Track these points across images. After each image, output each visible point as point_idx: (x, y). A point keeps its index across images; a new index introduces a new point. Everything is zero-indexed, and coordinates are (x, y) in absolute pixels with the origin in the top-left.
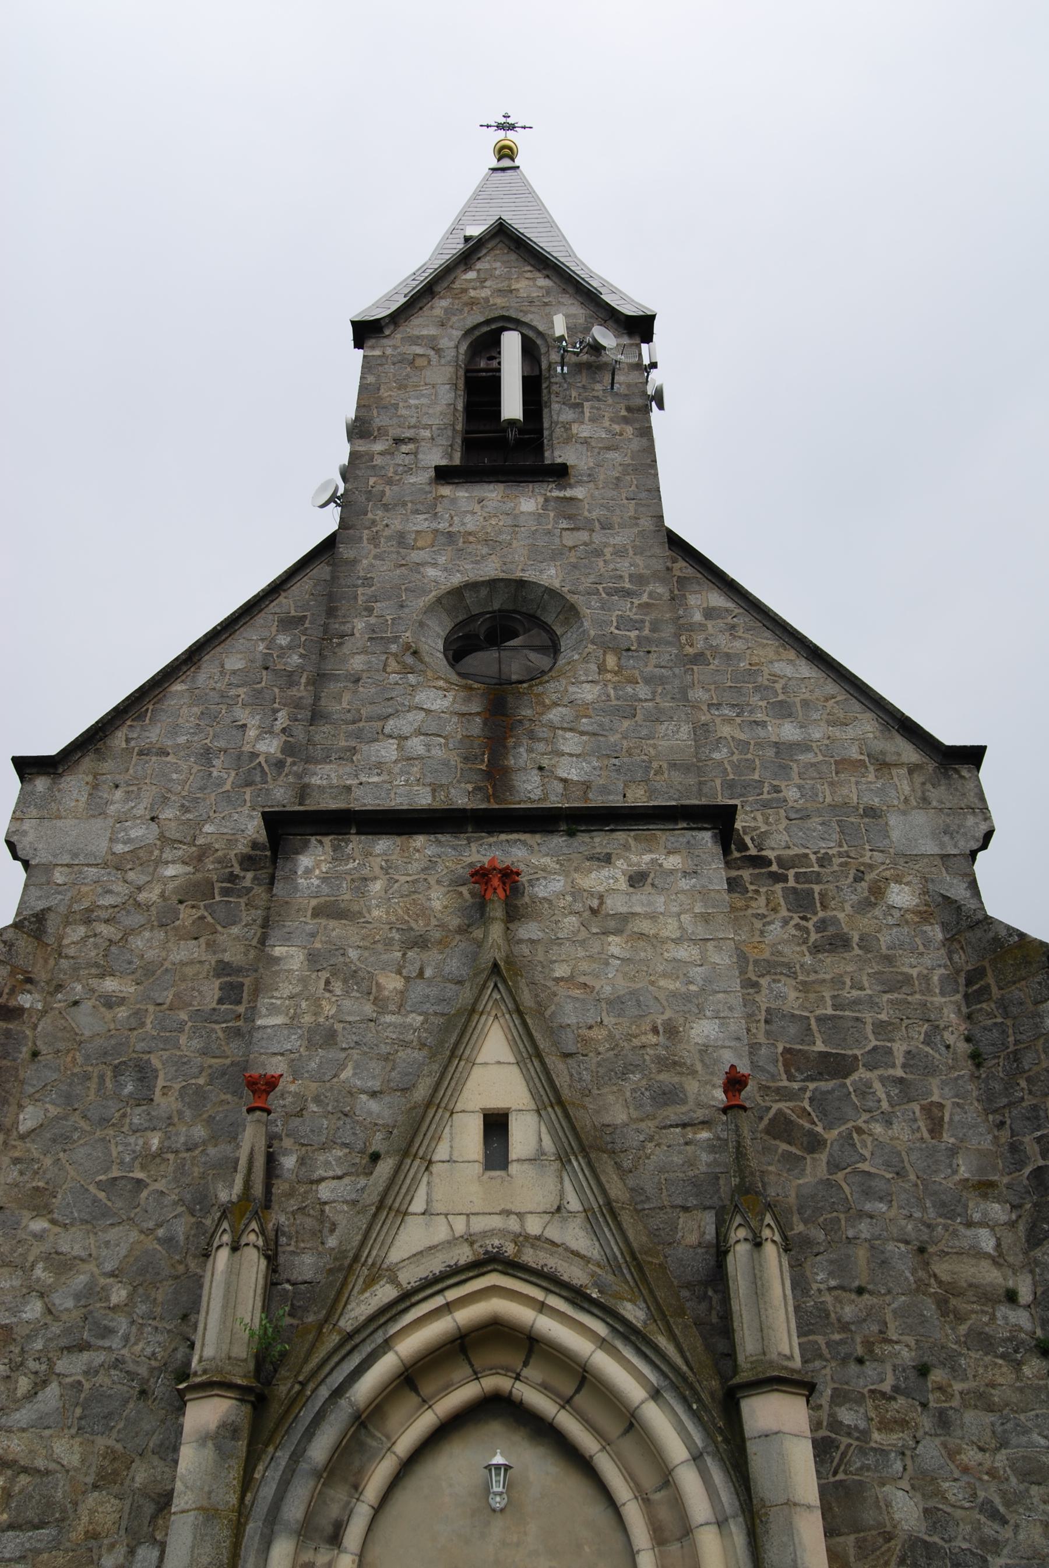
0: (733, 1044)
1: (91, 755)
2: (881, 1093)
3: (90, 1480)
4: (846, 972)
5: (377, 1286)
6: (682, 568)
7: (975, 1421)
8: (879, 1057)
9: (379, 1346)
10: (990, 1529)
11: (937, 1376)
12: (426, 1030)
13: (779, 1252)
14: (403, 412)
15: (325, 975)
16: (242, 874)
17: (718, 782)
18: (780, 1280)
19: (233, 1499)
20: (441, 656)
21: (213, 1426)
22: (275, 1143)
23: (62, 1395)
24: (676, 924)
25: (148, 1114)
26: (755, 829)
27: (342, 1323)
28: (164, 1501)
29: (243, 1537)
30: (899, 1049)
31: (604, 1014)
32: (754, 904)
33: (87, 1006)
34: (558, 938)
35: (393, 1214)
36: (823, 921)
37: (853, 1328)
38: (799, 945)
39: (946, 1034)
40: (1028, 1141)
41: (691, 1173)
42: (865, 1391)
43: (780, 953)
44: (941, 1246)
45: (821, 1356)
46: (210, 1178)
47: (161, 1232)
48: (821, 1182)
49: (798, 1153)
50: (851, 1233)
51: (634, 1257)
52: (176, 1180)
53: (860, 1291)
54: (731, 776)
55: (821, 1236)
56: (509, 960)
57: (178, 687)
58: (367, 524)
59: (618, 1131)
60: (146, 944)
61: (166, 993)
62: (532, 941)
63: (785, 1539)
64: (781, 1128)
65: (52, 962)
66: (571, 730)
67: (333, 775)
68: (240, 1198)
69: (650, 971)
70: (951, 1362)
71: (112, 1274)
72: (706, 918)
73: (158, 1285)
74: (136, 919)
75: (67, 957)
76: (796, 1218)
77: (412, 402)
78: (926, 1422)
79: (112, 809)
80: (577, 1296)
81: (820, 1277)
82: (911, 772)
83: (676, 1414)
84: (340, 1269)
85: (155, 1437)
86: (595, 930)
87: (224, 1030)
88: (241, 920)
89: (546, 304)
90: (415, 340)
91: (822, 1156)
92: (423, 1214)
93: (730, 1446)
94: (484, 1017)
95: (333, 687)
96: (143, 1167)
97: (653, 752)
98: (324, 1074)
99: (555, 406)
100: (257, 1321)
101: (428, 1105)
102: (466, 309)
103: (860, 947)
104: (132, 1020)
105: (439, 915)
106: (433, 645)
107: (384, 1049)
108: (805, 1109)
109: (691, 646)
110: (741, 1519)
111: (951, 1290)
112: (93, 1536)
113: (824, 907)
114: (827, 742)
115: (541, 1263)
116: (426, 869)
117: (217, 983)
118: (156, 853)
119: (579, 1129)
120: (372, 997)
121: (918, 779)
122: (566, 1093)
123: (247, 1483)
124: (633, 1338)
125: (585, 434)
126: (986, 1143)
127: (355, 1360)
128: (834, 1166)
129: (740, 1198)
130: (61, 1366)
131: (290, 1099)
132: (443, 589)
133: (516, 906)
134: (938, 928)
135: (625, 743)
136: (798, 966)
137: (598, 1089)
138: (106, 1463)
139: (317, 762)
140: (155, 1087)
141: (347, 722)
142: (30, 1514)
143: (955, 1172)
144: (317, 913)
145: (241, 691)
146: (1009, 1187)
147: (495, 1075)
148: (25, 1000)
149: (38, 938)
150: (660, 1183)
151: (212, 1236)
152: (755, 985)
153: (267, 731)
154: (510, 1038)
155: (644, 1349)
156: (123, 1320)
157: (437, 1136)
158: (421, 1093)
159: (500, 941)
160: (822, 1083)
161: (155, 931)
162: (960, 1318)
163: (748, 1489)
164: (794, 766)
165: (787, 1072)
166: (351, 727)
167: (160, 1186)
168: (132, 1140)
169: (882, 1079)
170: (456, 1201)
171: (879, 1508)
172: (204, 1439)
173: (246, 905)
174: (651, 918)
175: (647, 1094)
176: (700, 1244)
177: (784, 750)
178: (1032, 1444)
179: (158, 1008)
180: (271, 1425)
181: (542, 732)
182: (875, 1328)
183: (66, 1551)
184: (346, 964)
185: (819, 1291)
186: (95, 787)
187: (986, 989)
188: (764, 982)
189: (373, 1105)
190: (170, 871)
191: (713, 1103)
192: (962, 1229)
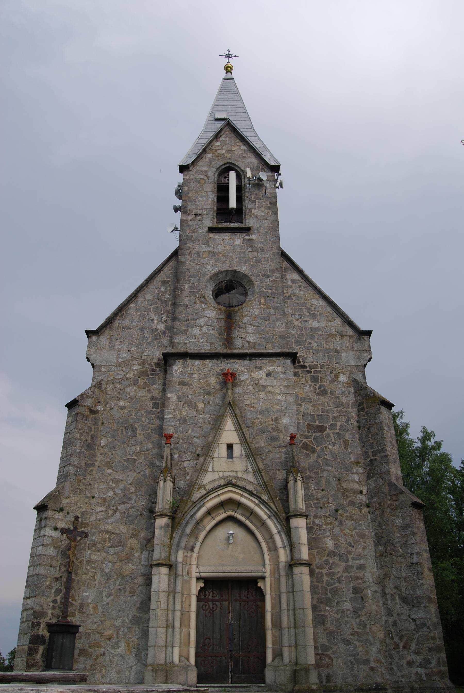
0: (293, 424)
1: (108, 329)
2: (332, 437)
3: (130, 536)
6: (286, 264)
7: (349, 523)
10: (350, 549)
11: (340, 512)
15: (182, 403)
16: (156, 369)
17: (293, 340)
19: (169, 542)
20: (211, 297)
27: (192, 499)
30: (338, 424)
32: (301, 380)
33: (116, 409)
36: (321, 386)
39: (352, 420)
43: (308, 396)
44: (344, 479)
45: (311, 507)
48: (315, 461)
50: (321, 475)
51: (265, 483)
52: (145, 459)
53: (323, 490)
54: (297, 339)
55: (313, 475)
56: (233, 402)
57: (132, 306)
60: (130, 390)
62: (239, 393)
65: (104, 396)
66: (251, 325)
67: (181, 339)
70: (344, 508)
71: (130, 484)
72: (287, 387)
75: (108, 394)
76: (307, 471)
77: (200, 199)
78: (336, 523)
79: (116, 347)
80: (251, 493)
81: (313, 486)
82: (349, 338)
87: (155, 417)
89: (244, 157)
90: (200, 172)
93: (287, 530)
95: (180, 309)
96: (136, 455)
97: (274, 333)
99: (247, 202)
100: (171, 499)
102: (217, 159)
105: (213, 385)
106: (209, 293)
107: (200, 425)
109: (287, 293)
111: (346, 490)
114: (326, 327)
116: (209, 370)
117: (151, 402)
118: (131, 362)
121: (352, 340)
122: (248, 440)
123: (171, 538)
125: (256, 214)
126: (359, 451)
127: (196, 508)
128: (318, 457)
129: (291, 468)
130: (119, 508)
132: (212, 273)
133: (235, 383)
134: (352, 388)
135: (266, 329)
139: (177, 335)
141: (185, 321)
142: (116, 544)
143: (350, 459)
144: (179, 384)
145: (151, 307)
147: (229, 434)
148: (99, 408)
149: (100, 389)
152: (300, 405)
153: (160, 321)
159: (231, 395)
162: (347, 497)
163: (291, 540)
164: (316, 335)
165: (308, 430)
166: (186, 323)
167: (140, 461)
168: (132, 448)
169: (333, 433)
170: (219, 467)
172: (161, 528)
177: (313, 330)
178: (362, 529)
181: (242, 326)
182: (326, 500)
185: (312, 490)
186: (111, 340)
187: (363, 408)
189: (197, 441)
190: (135, 367)
192: (350, 475)
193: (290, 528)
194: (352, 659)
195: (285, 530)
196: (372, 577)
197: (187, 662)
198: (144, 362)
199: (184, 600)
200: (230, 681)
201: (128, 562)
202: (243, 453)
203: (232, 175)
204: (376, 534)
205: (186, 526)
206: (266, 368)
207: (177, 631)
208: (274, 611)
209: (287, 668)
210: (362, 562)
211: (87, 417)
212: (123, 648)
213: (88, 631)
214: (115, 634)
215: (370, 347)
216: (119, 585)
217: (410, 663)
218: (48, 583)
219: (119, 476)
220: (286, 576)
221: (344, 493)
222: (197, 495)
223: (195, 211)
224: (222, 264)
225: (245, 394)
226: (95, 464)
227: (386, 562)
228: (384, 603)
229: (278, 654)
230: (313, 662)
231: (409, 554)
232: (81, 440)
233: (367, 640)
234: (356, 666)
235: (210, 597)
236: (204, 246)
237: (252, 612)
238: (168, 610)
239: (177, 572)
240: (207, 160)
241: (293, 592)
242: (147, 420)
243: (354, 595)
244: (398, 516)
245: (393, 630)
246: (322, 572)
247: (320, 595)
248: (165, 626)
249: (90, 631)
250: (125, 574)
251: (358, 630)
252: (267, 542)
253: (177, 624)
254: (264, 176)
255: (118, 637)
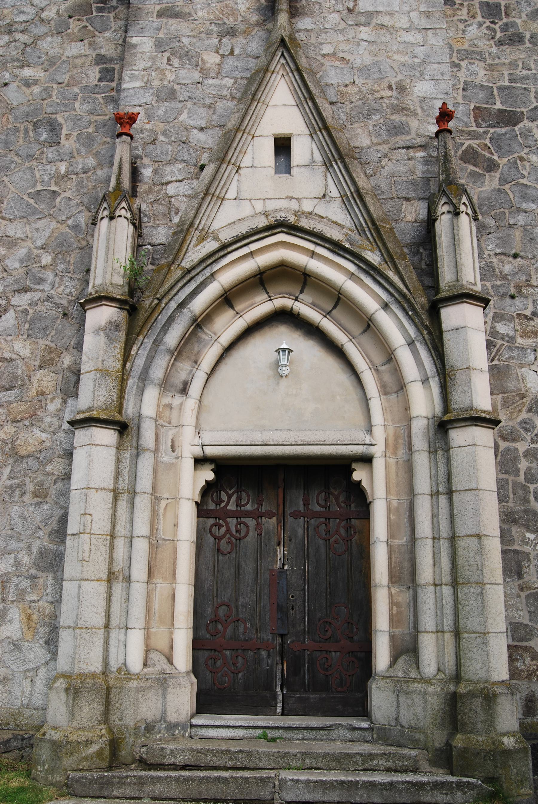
3: (37, 363)
4: (519, 58)
5: (206, 242)
9: (208, 278)
12: (235, 88)
13: (470, 221)
15: (166, 55)
18: (470, 238)
19: (118, 365)
21: (103, 323)
22: (138, 161)
23: (16, 317)
24: (407, 19)
25: (58, 151)
27: (183, 264)
29: (126, 387)
31: (356, 77)
32: (459, 13)
33: (13, 87)
34: (325, 28)
35: (215, 198)
36: (506, 24)
37: (509, 278)
38: (489, 40)
41: (411, 178)
42: (515, 314)
43: (475, 45)
46: (99, 189)
47: (70, 222)
48: (495, 190)
49: (481, 172)
50: (511, 222)
52: (77, 190)
53: (515, 256)
56: (292, 38)
59: (364, 151)
60: (50, 45)
61: (64, 76)
62: (307, 30)
63: (466, 388)
64: (471, 156)
68: (115, 190)
69: (388, 49)
71: (42, 248)
72: (428, 15)
73: (70, 253)
74: (41, 29)
80: (336, 247)
83: (398, 318)
84: (181, 231)
85: (74, 339)
86: (350, 23)
87: (104, 98)
88: (111, 27)
91: (496, 174)
92: (235, 199)
93: (434, 338)
94: (274, 76)
96: (56, 184)
98: (169, 117)
101: (237, 130)
103: (530, 42)
104: (43, 93)
107: (208, 101)
108: (487, 145)
110: (437, 379)
113: (507, 15)
115: (312, 227)
117: (97, 69)
119: (338, 144)
120: (199, 68)
122: (330, 122)
123: (126, 357)
124: (372, 272)
127: (193, 286)
128: (504, 180)
129: (442, 189)
131: (146, 134)
133: (297, 8)
136: (487, 54)
137: (351, 124)
138: (46, 354)
140: (61, 134)
144: (160, 14)
147: (281, 111)
150: (391, 183)
151: (97, 212)
154: (292, 88)
155: (379, 279)
156: (50, 273)
157: (243, 151)
159: (286, 25)
160: (499, 129)
161: (55, 37)
165: (476, 121)
167: (68, 194)
168: (48, 167)
170: (255, 189)
171: (518, 380)
172: (98, 331)
173: (114, 18)
174: (389, 14)
175: (384, 128)
176: (416, 221)
179: (60, 86)
182: (524, 278)
183: (26, 402)
184: (181, 47)
188: (463, 64)
191: (427, 134)
193: (441, 332)
195: (427, 337)
199: (161, 511)
200: (279, 710)
201: (33, 425)
205: (165, 328)
207: (138, 590)
208: (396, 542)
209: (431, 689)
212: (16, 625)
216: (9, 478)
220: (430, 452)
222: (194, 254)
229: (407, 649)
230: (505, 675)
235: (232, 507)
237: (336, 542)
238: (113, 536)
239: (141, 442)
241: (450, 493)
242: (86, 107)
246: (516, 449)
247: (511, 504)
248: (105, 577)
250: (23, 453)
252: (377, 370)
253: (139, 572)
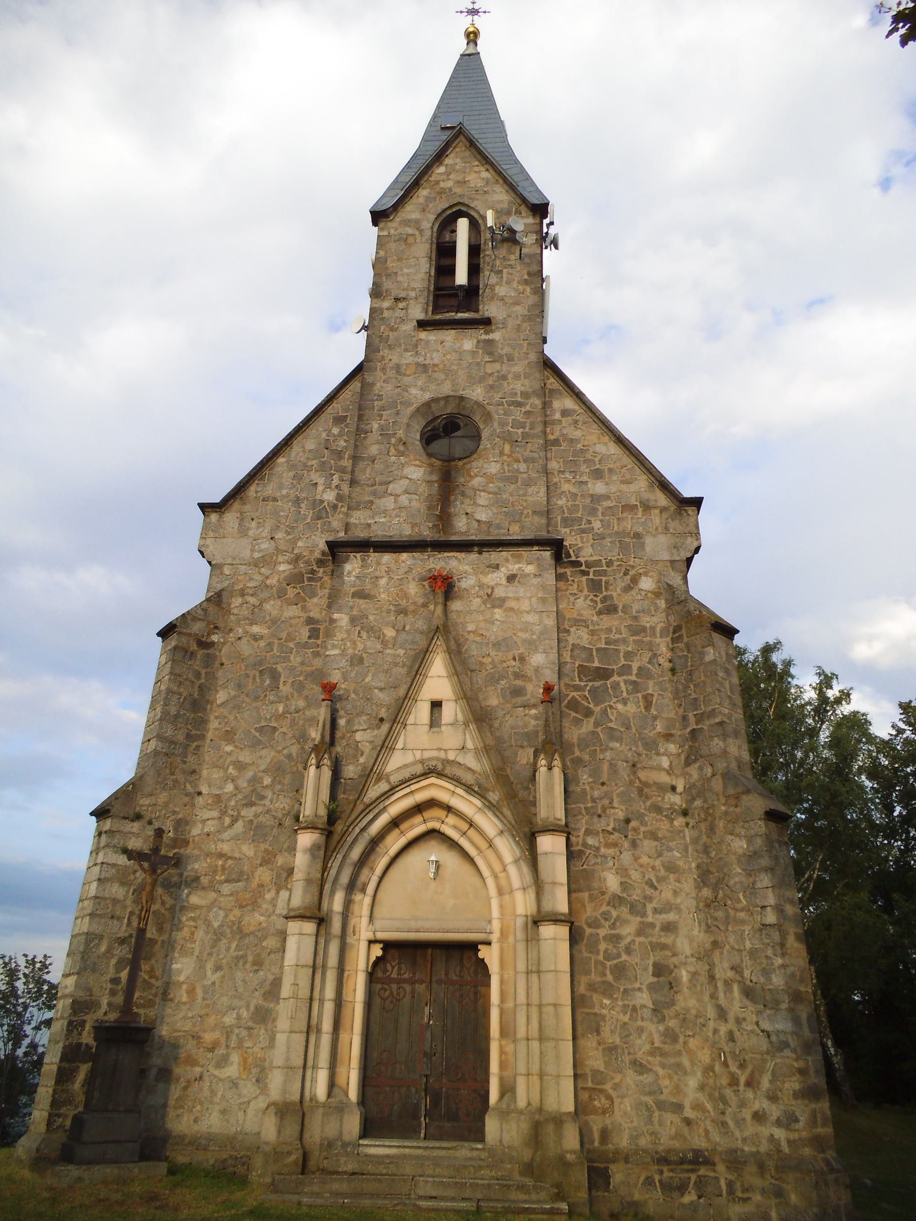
3: (259, 862)
6: (553, 383)
7: (648, 845)
8: (625, 670)
10: (649, 891)
11: (633, 824)
14: (400, 278)
15: (358, 628)
17: (559, 518)
19: (319, 876)
20: (418, 443)
26: (577, 545)
28: (291, 871)
30: (635, 666)
32: (570, 588)
33: (244, 640)
40: (691, 715)
43: (581, 615)
44: (644, 764)
47: (285, 752)
52: (291, 726)
53: (603, 784)
55: (586, 757)
57: (281, 460)
58: (380, 358)
66: (483, 491)
70: (641, 817)
71: (263, 772)
76: (576, 749)
77: (405, 270)
78: (626, 844)
79: (251, 533)
80: (469, 788)
82: (661, 512)
84: (364, 776)
90: (406, 223)
93: (532, 857)
95: (361, 464)
96: (276, 720)
97: (525, 504)
99: (487, 273)
107: (386, 667)
111: (646, 784)
112: (261, 886)
114: (619, 494)
121: (665, 515)
123: (324, 869)
125: (502, 294)
127: (371, 816)
128: (597, 724)
130: (243, 813)
134: (663, 601)
143: (654, 729)
145: (314, 462)
146: (680, 736)
147: (438, 682)
148: (215, 638)
153: (328, 486)
158: (402, 692)
165: (579, 676)
167: (284, 730)
169: (626, 682)
170: (416, 743)
177: (596, 499)
178: (673, 856)
180: (335, 844)
181: (469, 492)
186: (242, 520)
187: (681, 636)
189: (381, 695)
190: (282, 568)
192: (654, 757)
194: (649, 1100)
196: (691, 945)
197: (343, 1098)
198: (297, 559)
200: (422, 1135)
201: (254, 910)
202: (460, 717)
203: (463, 225)
204: (698, 867)
206: (507, 567)
210: (671, 917)
211: (192, 653)
213: (176, 1034)
214: (223, 1040)
215: (697, 528)
217: (759, 1117)
218: (103, 948)
219: (245, 757)
221: (642, 790)
222: (373, 792)
223: (395, 293)
224: (438, 385)
225: (468, 613)
226: (204, 735)
227: (716, 919)
228: (713, 996)
229: (507, 1089)
230: (571, 1108)
231: (757, 906)
232: (180, 694)
233: (679, 1065)
234: (657, 1114)
236: (409, 354)
238: (311, 999)
240: (421, 200)
242: (299, 659)
243: (655, 979)
244: (739, 836)
245: (726, 1049)
249: (180, 1034)
251: (662, 1046)
254: (520, 223)
255: (227, 1046)
